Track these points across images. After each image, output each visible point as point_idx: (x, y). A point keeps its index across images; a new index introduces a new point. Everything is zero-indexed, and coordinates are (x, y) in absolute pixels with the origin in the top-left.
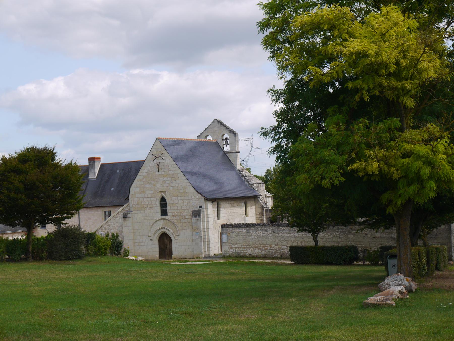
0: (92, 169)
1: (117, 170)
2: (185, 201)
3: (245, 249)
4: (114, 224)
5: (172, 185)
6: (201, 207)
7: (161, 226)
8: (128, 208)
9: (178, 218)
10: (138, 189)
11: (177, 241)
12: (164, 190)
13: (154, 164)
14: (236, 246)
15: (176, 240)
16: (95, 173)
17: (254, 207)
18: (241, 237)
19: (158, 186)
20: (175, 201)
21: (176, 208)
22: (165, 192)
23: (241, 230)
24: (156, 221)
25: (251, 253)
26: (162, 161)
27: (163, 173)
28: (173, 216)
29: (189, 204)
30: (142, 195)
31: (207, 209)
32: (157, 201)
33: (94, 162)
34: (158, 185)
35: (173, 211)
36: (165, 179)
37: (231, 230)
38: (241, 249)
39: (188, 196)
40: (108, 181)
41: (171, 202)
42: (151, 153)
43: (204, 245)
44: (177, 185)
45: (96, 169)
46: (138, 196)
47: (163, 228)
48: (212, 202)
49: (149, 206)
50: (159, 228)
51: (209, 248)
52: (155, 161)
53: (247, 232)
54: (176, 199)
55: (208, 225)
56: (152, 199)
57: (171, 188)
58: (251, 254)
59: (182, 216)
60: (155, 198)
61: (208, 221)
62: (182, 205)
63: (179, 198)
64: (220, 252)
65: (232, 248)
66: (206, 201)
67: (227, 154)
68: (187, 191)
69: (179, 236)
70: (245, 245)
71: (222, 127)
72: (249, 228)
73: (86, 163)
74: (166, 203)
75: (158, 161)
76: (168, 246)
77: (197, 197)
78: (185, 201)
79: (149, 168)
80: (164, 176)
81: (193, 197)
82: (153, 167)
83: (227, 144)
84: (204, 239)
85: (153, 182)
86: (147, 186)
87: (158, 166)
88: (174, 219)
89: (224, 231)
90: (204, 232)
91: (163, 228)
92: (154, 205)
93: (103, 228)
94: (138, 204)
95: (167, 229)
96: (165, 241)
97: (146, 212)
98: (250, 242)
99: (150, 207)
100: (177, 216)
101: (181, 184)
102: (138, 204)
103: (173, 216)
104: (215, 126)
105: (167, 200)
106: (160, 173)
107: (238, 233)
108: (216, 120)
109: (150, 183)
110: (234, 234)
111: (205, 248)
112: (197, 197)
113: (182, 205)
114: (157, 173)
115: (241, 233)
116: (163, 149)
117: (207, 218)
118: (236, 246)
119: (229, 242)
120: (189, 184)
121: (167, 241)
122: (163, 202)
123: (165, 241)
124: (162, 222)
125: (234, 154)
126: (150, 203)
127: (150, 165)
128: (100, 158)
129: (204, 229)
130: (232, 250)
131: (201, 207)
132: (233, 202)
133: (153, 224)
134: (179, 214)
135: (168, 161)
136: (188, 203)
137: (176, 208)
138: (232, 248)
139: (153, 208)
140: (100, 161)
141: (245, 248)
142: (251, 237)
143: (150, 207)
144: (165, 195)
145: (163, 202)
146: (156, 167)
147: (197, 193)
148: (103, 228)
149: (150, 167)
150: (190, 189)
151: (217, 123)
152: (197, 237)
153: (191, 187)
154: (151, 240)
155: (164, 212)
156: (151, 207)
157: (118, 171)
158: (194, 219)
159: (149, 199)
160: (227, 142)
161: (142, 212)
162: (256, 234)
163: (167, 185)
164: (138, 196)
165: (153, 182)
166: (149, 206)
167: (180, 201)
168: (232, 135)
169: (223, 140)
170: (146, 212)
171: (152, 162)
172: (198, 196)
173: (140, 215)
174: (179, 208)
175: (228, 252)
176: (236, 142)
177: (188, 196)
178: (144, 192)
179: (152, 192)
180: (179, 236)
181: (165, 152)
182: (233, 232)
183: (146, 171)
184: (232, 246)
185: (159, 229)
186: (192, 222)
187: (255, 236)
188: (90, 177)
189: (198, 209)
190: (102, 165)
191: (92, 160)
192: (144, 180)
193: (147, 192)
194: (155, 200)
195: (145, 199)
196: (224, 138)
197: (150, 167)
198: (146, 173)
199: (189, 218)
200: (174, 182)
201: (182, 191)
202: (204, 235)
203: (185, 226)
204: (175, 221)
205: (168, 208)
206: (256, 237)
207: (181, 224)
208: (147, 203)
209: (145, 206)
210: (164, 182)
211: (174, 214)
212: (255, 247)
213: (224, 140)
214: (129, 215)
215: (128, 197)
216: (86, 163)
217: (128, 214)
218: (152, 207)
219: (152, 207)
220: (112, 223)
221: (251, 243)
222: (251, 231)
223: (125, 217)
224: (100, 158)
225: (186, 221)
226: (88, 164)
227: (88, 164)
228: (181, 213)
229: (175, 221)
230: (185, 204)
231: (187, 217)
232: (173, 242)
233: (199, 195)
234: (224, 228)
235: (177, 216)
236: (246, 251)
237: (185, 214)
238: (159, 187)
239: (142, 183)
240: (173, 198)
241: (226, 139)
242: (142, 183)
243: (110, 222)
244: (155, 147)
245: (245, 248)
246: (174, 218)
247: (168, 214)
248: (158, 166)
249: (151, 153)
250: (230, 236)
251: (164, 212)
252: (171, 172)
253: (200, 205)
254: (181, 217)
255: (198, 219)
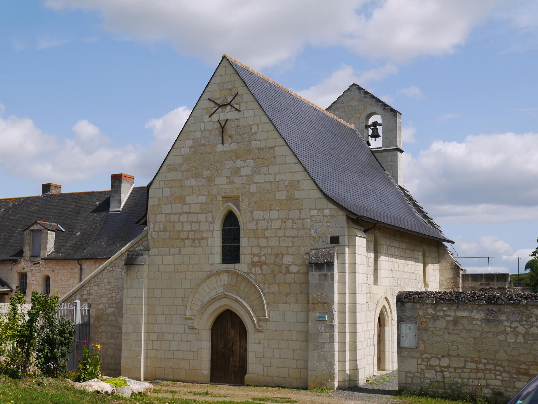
0: (116, 195)
2: (289, 223)
3: (480, 375)
4: (109, 283)
5: (258, 178)
6: (335, 240)
8: (145, 243)
10: (167, 192)
11: (261, 335)
12: (235, 193)
14: (445, 362)
15: (257, 331)
16: (120, 202)
17: (437, 266)
18: (463, 334)
19: (221, 181)
20: (264, 224)
21: (263, 242)
22: (236, 200)
23: (466, 314)
24: (208, 277)
25: (503, 389)
27: (235, 146)
28: (254, 264)
30: (178, 208)
31: (353, 246)
33: (121, 182)
35: (256, 250)
36: (240, 163)
37: (430, 311)
38: (465, 375)
39: (300, 210)
42: (207, 95)
43: (342, 351)
44: (269, 178)
45: (123, 195)
46: (166, 209)
47: (226, 297)
48: (365, 232)
49: (191, 235)
50: (213, 294)
51: (354, 360)
52: (215, 117)
53: (488, 321)
54: (266, 217)
55: (354, 293)
56: (202, 217)
57: (253, 188)
58: (500, 394)
59: (280, 266)
60: (210, 215)
61: (354, 283)
62: (281, 233)
63: (274, 214)
64: (376, 373)
65: (432, 367)
66: (352, 225)
67: (376, 155)
68: (298, 194)
70: (478, 363)
71: (368, 100)
72: (495, 308)
73: (106, 186)
74: (238, 230)
75: (222, 115)
76: (236, 348)
77: (327, 212)
79: (199, 134)
80: (237, 155)
82: (210, 131)
83: (375, 135)
84: (342, 333)
85: (206, 173)
86: (191, 182)
87: (223, 128)
89: (408, 314)
90: (342, 312)
92: (205, 235)
93: (85, 292)
94: (165, 230)
98: (496, 352)
99: (194, 240)
100: (264, 263)
101: (283, 177)
102: (165, 230)
103: (254, 264)
104: (352, 99)
105: (241, 221)
106: (227, 147)
107: (456, 322)
108: (354, 85)
109: (198, 176)
110: (441, 324)
111: (342, 361)
112: (327, 212)
113: (281, 233)
114: (219, 148)
115: (464, 321)
116: (239, 83)
117: (354, 272)
118: (445, 362)
119: (422, 347)
120: (302, 176)
121: (233, 333)
122: (231, 227)
125: (391, 153)
126: (195, 227)
127: (202, 126)
128: (132, 178)
129: (342, 304)
130: (430, 374)
131: (335, 240)
132: (404, 245)
134: (271, 259)
135: (250, 113)
136: (298, 229)
137: (263, 242)
138: (432, 367)
139: (203, 242)
141: (478, 370)
142: (502, 337)
144: (238, 207)
145: (231, 227)
146: (218, 132)
147: (325, 201)
148: (85, 292)
149: (202, 131)
150: (307, 191)
151: (357, 92)
153: (310, 185)
155: (231, 253)
159: (192, 218)
160: (375, 131)
161: (173, 250)
162: (521, 329)
163: (244, 180)
164: (166, 209)
165: (206, 173)
166: (191, 235)
167: (277, 224)
168: (389, 113)
169: (367, 127)
170: (184, 251)
171: (206, 118)
172: (329, 209)
173: (168, 259)
174: (274, 242)
175: (416, 381)
176: (392, 133)
178: (182, 200)
179: (203, 199)
181: (242, 90)
182: (436, 318)
184: (434, 362)
185: (214, 300)
186: (307, 282)
187: (516, 334)
191: (117, 179)
192: (185, 167)
194: (210, 219)
195: (183, 218)
196: (370, 122)
197: (202, 131)
198: (190, 148)
199: (298, 272)
200: (264, 170)
201: (282, 195)
202: (342, 323)
203: (287, 295)
204: (260, 278)
205: (244, 242)
206: (520, 339)
208: (187, 227)
209: (183, 235)
210: (236, 171)
211: (256, 259)
212: (519, 372)
213: (370, 126)
214: (140, 259)
215: (146, 214)
216: (106, 186)
217: (138, 255)
220: (106, 281)
221: (502, 355)
222: (504, 318)
223: (131, 261)
224: (132, 178)
225: (290, 278)
226: (110, 189)
227: (110, 189)
228: (277, 256)
229: (260, 278)
230: (289, 233)
231: (294, 269)
232: (251, 336)
233: (331, 206)
234: (408, 305)
236: (483, 382)
237: (288, 260)
240: (258, 215)
241: (375, 124)
243: (100, 276)
244: (216, 79)
245: (478, 370)
246: (258, 270)
247: (242, 258)
248: (223, 128)
250: (426, 330)
252: (255, 145)
253: (335, 234)
254: (277, 269)
255: (325, 275)
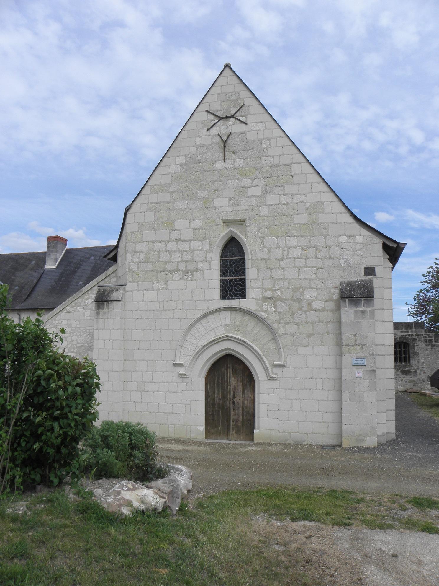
1: (91, 256)
2: (311, 252)
5: (270, 199)
6: (370, 271)
7: (221, 333)
9: (283, 307)
10: (150, 217)
11: (275, 384)
13: (210, 139)
15: (272, 379)
20: (279, 253)
21: (277, 274)
22: (241, 222)
24: (205, 316)
26: (240, 128)
27: (240, 163)
29: (328, 262)
32: (211, 250)
34: (217, 203)
35: (268, 284)
36: (246, 182)
39: (325, 236)
40: (74, 272)
41: (263, 255)
46: (150, 235)
47: (228, 338)
49: (182, 266)
50: (211, 337)
52: (214, 131)
54: (282, 243)
56: (195, 245)
57: (264, 211)
59: (299, 301)
62: (300, 263)
63: (292, 241)
68: (322, 218)
69: (283, 366)
75: (222, 128)
77: (359, 239)
78: (311, 252)
79: (193, 150)
81: (343, 239)
82: (208, 147)
85: (203, 194)
87: (225, 143)
88: (267, 311)
91: (228, 338)
92: (200, 266)
94: (146, 261)
95: (243, 343)
96: (229, 382)
97: (171, 285)
99: (185, 272)
102: (146, 261)
106: (229, 164)
113: (300, 263)
114: (220, 165)
121: (234, 382)
123: (229, 382)
124: (226, 318)
126: (187, 257)
127: (198, 141)
131: (370, 271)
133: (192, 326)
134: (288, 294)
136: (323, 258)
137: (277, 274)
139: (197, 275)
140: (66, 245)
143: (185, 272)
147: (356, 226)
149: (197, 147)
152: (360, 372)
154: (183, 376)
155: (233, 284)
156: (190, 271)
157: (93, 258)
158: (349, 312)
159: (184, 246)
161: (157, 285)
163: (252, 201)
164: (150, 235)
165: (203, 194)
166: (182, 266)
167: (295, 252)
170: (172, 285)
171: (204, 132)
173: (151, 295)
174: (291, 274)
177: (325, 236)
178: (170, 225)
179: (197, 223)
180: (283, 366)
183: (181, 160)
185: (213, 343)
188: (46, 267)
189: (359, 277)
190: (68, 251)
193: (178, 224)
194: (207, 247)
195: (171, 246)
197: (197, 147)
198: (181, 165)
199: (323, 309)
200: (278, 190)
201: (302, 219)
203: (309, 336)
205: (251, 273)
207: (293, 328)
208: (176, 257)
209: (169, 267)
210: (242, 191)
211: (268, 294)
217: (112, 291)
218: (192, 272)
219: (192, 272)
225: (312, 316)
226: (45, 249)
227: (45, 249)
228: (295, 290)
235: (280, 299)
237: (310, 295)
238: (223, 207)
239: (166, 197)
240: (270, 242)
242: (166, 197)
247: (249, 292)
248: (225, 143)
249: (203, 107)
251: (233, 284)
252: (265, 161)
253: (370, 265)
254: (295, 305)
255: (363, 312)
